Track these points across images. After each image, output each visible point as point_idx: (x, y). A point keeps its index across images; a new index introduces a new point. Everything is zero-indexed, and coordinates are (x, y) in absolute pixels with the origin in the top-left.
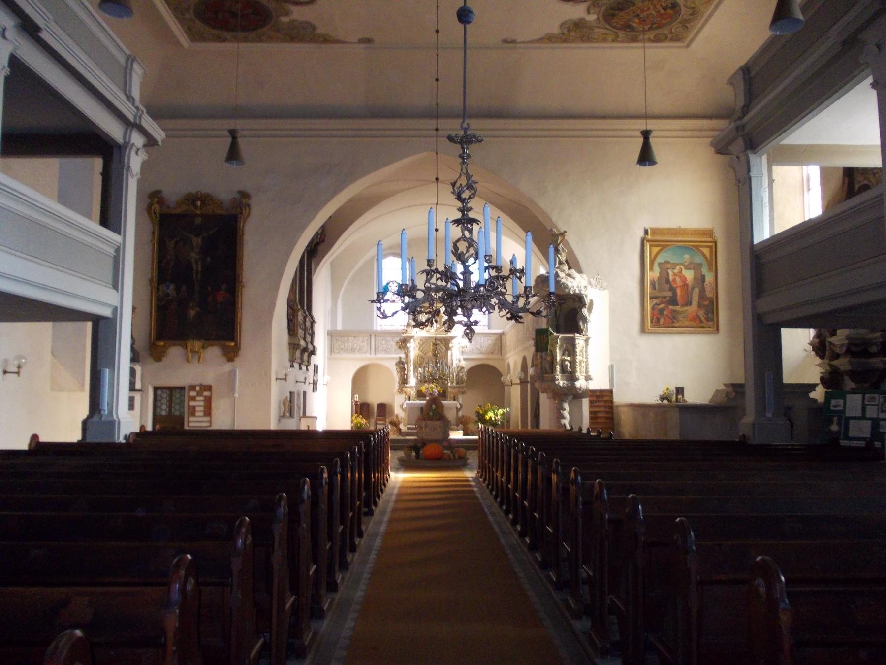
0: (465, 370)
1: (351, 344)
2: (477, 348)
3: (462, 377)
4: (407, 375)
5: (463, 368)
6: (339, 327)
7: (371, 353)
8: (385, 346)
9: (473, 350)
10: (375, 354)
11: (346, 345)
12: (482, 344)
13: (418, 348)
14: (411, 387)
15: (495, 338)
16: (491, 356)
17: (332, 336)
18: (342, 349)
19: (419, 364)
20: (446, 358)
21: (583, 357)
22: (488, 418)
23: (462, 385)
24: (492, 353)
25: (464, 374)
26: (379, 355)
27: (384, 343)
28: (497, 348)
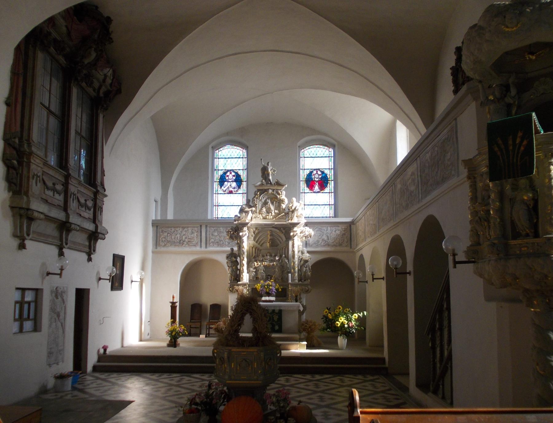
0: (310, 264)
1: (178, 235)
2: (323, 240)
3: (305, 272)
4: (240, 270)
5: (306, 261)
6: (170, 216)
7: (201, 247)
9: (318, 241)
10: (206, 247)
11: (173, 237)
13: (252, 238)
14: (244, 285)
15: (343, 227)
16: (338, 249)
17: (157, 226)
18: (168, 242)
20: (286, 249)
23: (306, 283)
24: (340, 245)
25: (308, 269)
26: (210, 249)
27: (216, 234)
28: (346, 240)
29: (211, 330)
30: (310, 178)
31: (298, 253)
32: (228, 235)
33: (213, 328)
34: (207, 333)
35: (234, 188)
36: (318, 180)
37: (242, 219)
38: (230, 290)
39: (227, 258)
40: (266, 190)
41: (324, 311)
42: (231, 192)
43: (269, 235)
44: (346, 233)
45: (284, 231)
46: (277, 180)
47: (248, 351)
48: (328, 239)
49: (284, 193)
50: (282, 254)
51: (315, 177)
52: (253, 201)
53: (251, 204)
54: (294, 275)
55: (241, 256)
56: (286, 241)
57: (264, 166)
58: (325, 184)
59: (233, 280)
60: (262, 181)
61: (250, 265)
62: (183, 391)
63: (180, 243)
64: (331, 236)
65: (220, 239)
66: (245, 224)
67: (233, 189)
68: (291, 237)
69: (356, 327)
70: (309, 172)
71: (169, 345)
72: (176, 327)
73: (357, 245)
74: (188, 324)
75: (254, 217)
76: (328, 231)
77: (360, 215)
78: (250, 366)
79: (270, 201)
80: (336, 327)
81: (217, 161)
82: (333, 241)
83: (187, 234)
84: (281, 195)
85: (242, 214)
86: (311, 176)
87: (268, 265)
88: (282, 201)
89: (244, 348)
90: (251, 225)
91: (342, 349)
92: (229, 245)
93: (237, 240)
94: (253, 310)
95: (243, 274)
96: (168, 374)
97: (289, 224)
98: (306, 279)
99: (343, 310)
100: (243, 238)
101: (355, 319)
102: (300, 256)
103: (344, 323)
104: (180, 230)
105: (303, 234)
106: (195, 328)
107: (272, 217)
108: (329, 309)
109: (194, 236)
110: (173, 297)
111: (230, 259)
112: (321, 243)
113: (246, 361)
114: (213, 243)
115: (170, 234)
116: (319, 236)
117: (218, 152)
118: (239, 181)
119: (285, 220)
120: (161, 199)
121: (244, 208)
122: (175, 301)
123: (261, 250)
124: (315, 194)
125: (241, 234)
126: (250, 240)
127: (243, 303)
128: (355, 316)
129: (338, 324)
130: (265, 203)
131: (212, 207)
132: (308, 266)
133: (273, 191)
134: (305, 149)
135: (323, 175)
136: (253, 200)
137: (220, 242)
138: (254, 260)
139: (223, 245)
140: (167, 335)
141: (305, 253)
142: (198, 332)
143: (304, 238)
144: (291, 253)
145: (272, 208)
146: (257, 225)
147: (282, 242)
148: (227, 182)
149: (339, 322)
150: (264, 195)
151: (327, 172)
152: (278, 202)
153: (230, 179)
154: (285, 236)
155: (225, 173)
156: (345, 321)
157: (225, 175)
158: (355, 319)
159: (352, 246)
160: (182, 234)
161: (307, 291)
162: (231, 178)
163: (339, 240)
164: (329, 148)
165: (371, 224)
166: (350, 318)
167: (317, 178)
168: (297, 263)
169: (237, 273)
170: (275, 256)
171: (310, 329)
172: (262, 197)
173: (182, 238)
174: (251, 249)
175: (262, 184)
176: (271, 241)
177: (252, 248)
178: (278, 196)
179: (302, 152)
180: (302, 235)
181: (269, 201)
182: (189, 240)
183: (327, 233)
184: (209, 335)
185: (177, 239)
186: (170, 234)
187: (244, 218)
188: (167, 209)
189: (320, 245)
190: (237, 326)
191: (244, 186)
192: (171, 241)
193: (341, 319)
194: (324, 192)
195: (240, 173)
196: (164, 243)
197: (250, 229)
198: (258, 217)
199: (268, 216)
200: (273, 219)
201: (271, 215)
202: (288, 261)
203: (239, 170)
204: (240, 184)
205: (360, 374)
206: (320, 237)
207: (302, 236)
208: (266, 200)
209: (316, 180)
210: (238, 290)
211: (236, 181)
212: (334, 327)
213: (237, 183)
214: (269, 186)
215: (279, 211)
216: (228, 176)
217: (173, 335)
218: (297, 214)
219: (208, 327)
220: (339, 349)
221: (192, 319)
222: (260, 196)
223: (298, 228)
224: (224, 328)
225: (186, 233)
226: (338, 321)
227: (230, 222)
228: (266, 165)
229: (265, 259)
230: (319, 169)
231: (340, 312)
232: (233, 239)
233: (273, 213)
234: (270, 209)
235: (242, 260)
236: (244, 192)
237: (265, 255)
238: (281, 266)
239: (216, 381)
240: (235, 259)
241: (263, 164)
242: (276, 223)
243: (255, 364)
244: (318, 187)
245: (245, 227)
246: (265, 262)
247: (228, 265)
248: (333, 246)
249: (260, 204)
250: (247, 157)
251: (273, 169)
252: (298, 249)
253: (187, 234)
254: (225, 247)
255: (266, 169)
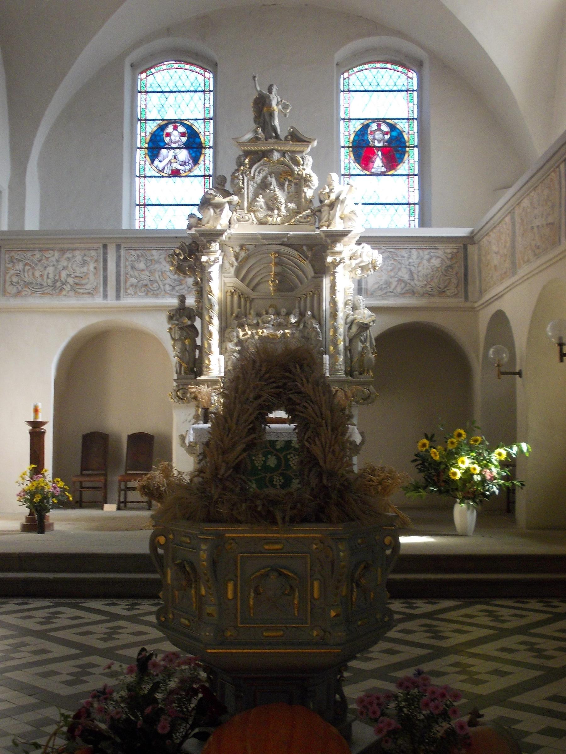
0: (374, 332)
1: (51, 270)
2: (400, 280)
3: (362, 354)
4: (201, 348)
5: (364, 327)
7: (105, 296)
8: (145, 275)
9: (388, 283)
10: (118, 297)
11: (37, 274)
12: (413, 268)
13: (232, 270)
14: (212, 382)
16: (437, 301)
18: (27, 284)
19: (237, 317)
20: (316, 297)
21: (283, 470)
22: (459, 476)
23: (362, 378)
24: (441, 293)
25: (368, 344)
26: (128, 301)
27: (142, 265)
28: (454, 281)
29: (129, 493)
30: (363, 140)
31: (345, 307)
32: (172, 262)
33: (138, 489)
34: (122, 500)
35: (184, 164)
36: (381, 144)
37: (208, 222)
38: (178, 396)
39: (171, 318)
40: (266, 154)
41: (418, 442)
42: (176, 174)
43: (273, 263)
44: (454, 264)
45: (309, 254)
46: (292, 128)
47: (287, 539)
48: (412, 279)
49: (309, 160)
50: (305, 311)
51: (374, 139)
52: (233, 180)
53: (228, 187)
54: (336, 360)
55: (205, 313)
56: (314, 277)
57: (259, 95)
58: (397, 156)
59: (185, 372)
60: (256, 132)
61: (226, 335)
62: (59, 651)
63: (54, 287)
64: (418, 272)
65: (152, 278)
66: (215, 235)
67: (181, 165)
68: (329, 267)
69: (501, 482)
70: (360, 127)
71: (26, 528)
72: (43, 482)
73: (481, 293)
74: (74, 479)
75: (237, 219)
76: (411, 260)
77: (495, 215)
78: (297, 595)
79: (277, 180)
80: (450, 482)
81: (143, 99)
82: (425, 283)
83: (72, 265)
84: (301, 167)
85: (206, 211)
86: (366, 135)
87: (271, 337)
88: (306, 180)
89: (275, 528)
90: (229, 238)
91: (464, 535)
92: (174, 293)
93: (194, 274)
94: (300, 393)
95: (210, 357)
96: (20, 600)
97: (322, 234)
98: (364, 371)
99: (469, 437)
100: (209, 270)
101: (501, 462)
102: (348, 315)
103: (472, 471)
104: (53, 256)
105: (357, 261)
106: (93, 488)
107: (281, 220)
108: (430, 438)
109: (88, 270)
110: (36, 411)
111: (176, 322)
112: (396, 286)
113: (281, 574)
114: (136, 289)
115: (30, 266)
116: (391, 270)
117: (147, 76)
118: (195, 146)
119: (312, 227)
120: (10, 187)
121: (212, 196)
122: (40, 420)
123: (252, 301)
124: (375, 177)
125: (204, 259)
126: (225, 275)
127: (264, 370)
128: (500, 454)
129: (455, 474)
130: (264, 186)
131: (130, 207)
132: (369, 337)
133: (283, 156)
134: (350, 72)
135: (394, 134)
136: (234, 177)
137: (152, 285)
138: (236, 322)
139: (158, 292)
140: (21, 503)
141: (362, 307)
142: (100, 499)
143: (359, 271)
144: (328, 306)
145: (281, 196)
146: (243, 239)
147: (306, 280)
148: (166, 148)
149: (459, 468)
150: (261, 165)
151: (402, 126)
152: (296, 184)
153: (175, 143)
154: (313, 266)
155: (162, 128)
156: (476, 466)
157: (161, 133)
158: (501, 462)
159: (469, 294)
160: (60, 267)
161: (367, 399)
162: (178, 139)
163: (439, 280)
164: (408, 69)
165: (538, 226)
166: (485, 459)
167: (379, 141)
168: (341, 330)
169: (195, 356)
170: (288, 314)
171: (380, 488)
172: (255, 171)
173: (60, 276)
174: (229, 298)
175: (256, 139)
176: (277, 278)
177: (232, 293)
178: (296, 169)
179: (344, 79)
180: (354, 262)
181: (273, 180)
182: (77, 280)
183: (410, 263)
184: (125, 506)
185: (48, 278)
186: (30, 266)
187: (211, 222)
188: (23, 210)
189: (393, 292)
190: (244, 450)
191: (207, 157)
192: (33, 283)
193: (463, 462)
194: (396, 173)
195: (199, 127)
196: (15, 288)
197: (226, 248)
198: (247, 218)
199: (270, 216)
200: (283, 223)
201: (279, 215)
202: (321, 327)
203: (196, 120)
204: (198, 154)
205: (532, 597)
206: (392, 274)
207: (353, 266)
208: (265, 178)
209: (377, 144)
210: (199, 396)
211: (187, 146)
212: (444, 481)
213: (191, 152)
214: (273, 144)
215: (298, 204)
216: (168, 135)
217: (35, 503)
218: (342, 212)
219: (123, 487)
220: (457, 535)
221: (83, 468)
222: (250, 168)
223: (344, 245)
224: (166, 485)
225: (70, 265)
226: (455, 465)
227: (176, 237)
228: (264, 92)
229: (264, 323)
230: (384, 120)
231: (460, 443)
232: (185, 274)
233: (283, 208)
234: (276, 199)
235: (206, 324)
236: (207, 173)
237: (264, 313)
238: (303, 337)
239: (169, 647)
240: (189, 323)
241: (258, 89)
242: (291, 233)
243: (316, 584)
244: (383, 162)
245: (215, 241)
246: (262, 328)
247: (173, 336)
248: (423, 295)
249: (250, 187)
250: (215, 91)
251: (283, 101)
252: (345, 298)
253: (72, 265)
254: (163, 297)
255: (265, 101)
